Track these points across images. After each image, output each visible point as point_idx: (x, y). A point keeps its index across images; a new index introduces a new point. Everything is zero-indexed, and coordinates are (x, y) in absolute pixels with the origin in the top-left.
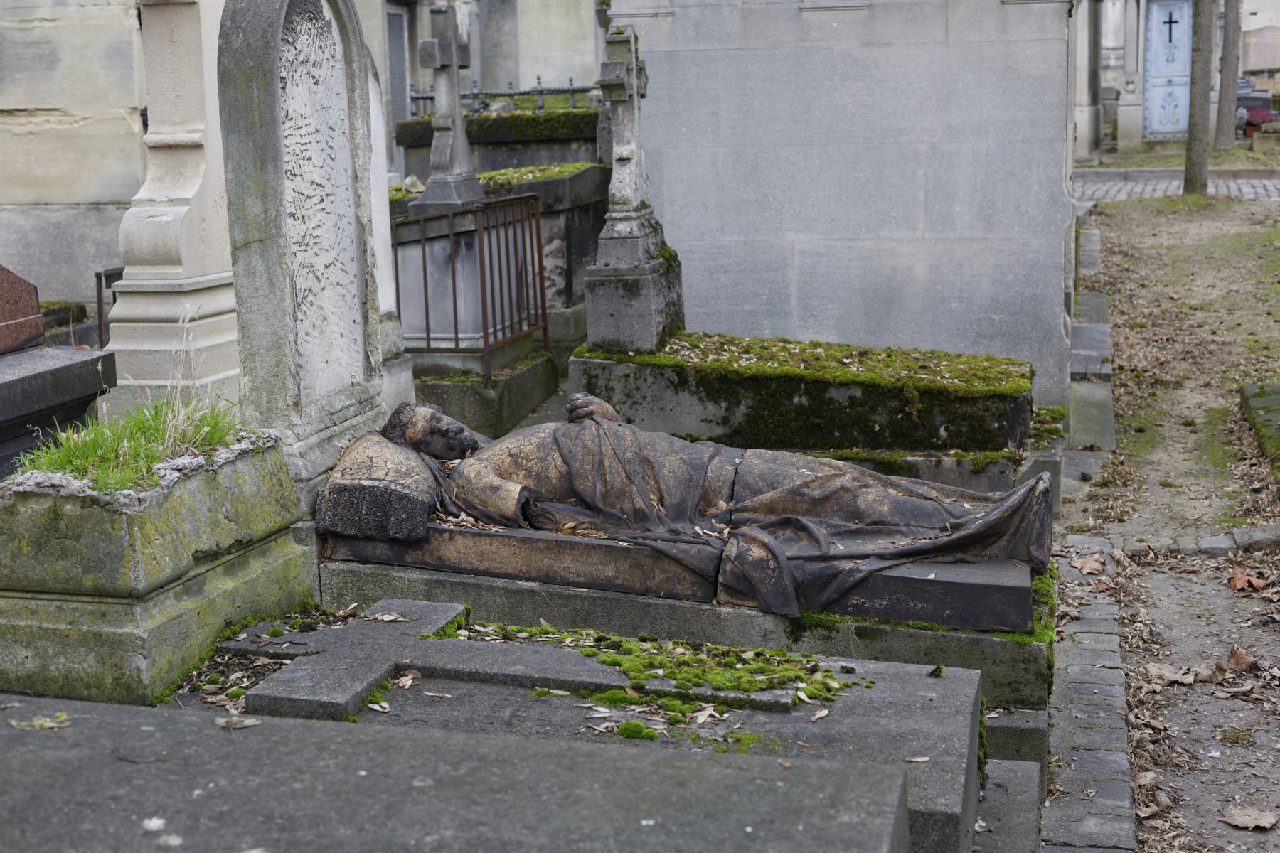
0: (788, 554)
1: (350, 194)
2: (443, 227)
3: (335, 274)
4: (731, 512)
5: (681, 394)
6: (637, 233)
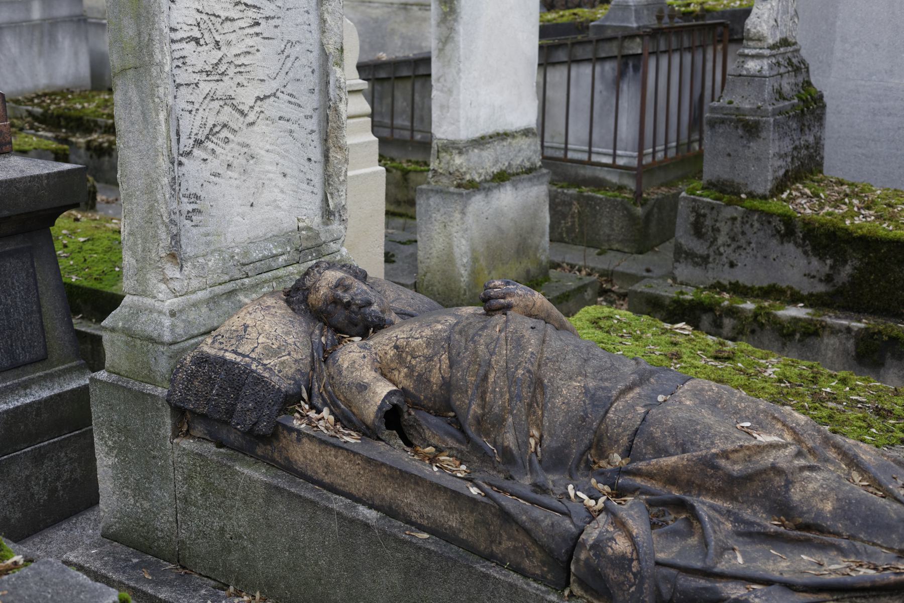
0: (661, 556)
1: (313, 18)
2: (612, 49)
4: (621, 472)
5: (786, 244)
6: (766, 72)
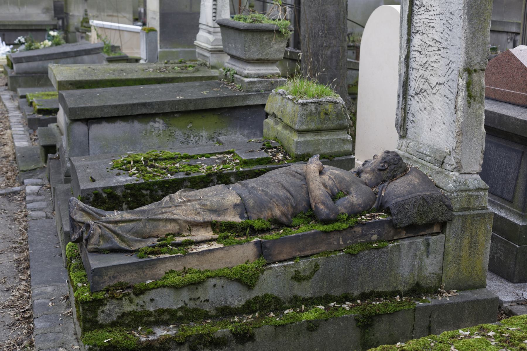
3: (443, 90)
